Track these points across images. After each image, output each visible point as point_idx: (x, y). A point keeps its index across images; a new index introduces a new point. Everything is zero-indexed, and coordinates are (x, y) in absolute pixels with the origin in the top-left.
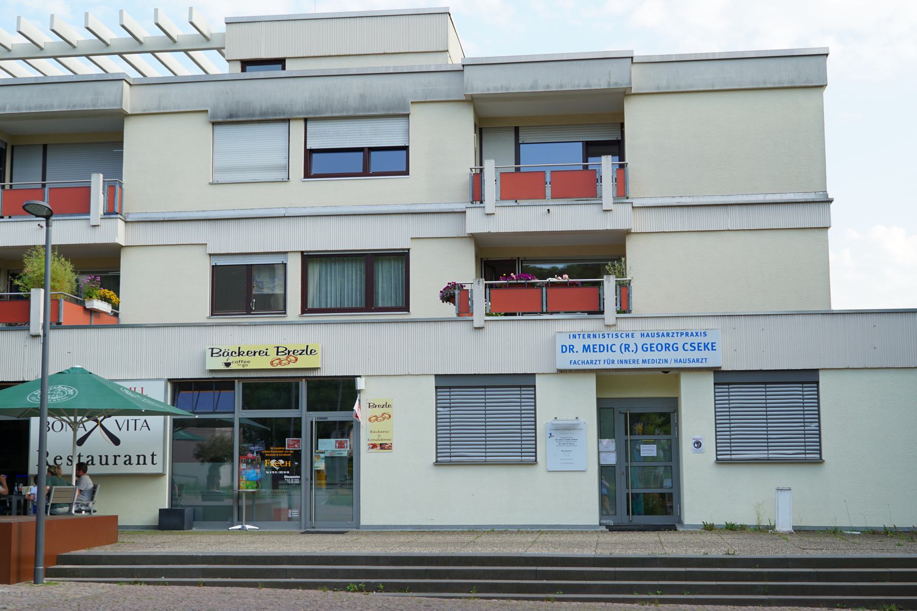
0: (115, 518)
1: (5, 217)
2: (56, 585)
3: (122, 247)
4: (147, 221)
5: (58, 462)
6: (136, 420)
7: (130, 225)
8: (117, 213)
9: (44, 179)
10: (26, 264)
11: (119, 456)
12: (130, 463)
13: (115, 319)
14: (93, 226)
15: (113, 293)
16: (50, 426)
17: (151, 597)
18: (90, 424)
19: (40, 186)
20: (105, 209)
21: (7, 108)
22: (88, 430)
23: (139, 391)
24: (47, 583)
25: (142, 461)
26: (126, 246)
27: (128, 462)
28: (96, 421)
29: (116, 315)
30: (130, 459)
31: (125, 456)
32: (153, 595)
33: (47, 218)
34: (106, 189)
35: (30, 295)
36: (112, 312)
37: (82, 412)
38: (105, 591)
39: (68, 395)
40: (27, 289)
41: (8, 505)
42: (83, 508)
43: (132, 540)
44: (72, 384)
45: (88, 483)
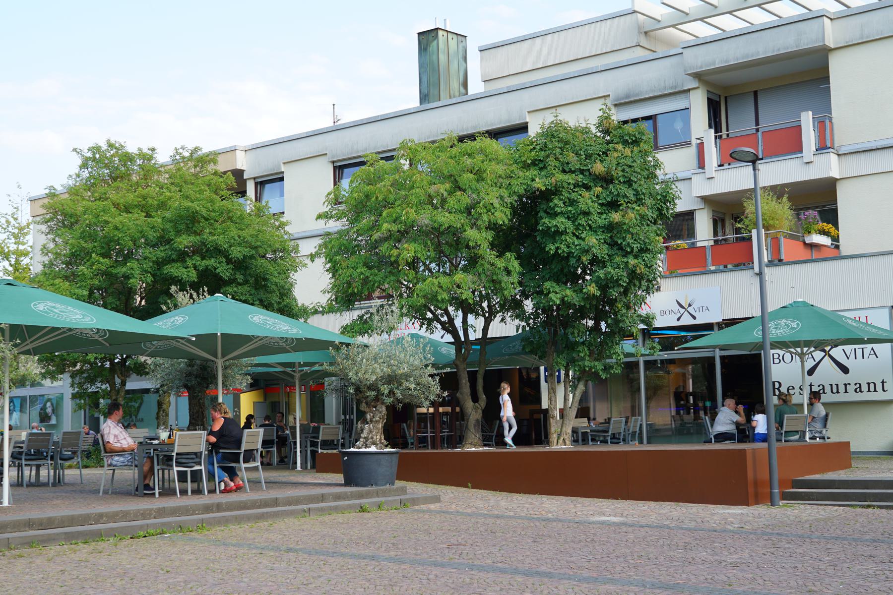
0: (847, 444)
1: (725, 165)
2: (792, 508)
3: (837, 180)
4: (859, 152)
5: (791, 392)
6: (863, 349)
7: (843, 157)
8: (830, 148)
9: (757, 124)
10: (745, 207)
11: (849, 384)
12: (861, 391)
13: (836, 250)
14: (806, 163)
15: (831, 226)
16: (781, 358)
17: (882, 520)
18: (818, 355)
19: (754, 131)
20: (817, 145)
21: (717, 63)
22: (817, 361)
23: (863, 320)
24: (783, 506)
25: (872, 389)
26: (840, 179)
27: (859, 389)
28: (824, 351)
29: (837, 247)
30: (860, 387)
31: (855, 384)
32: (885, 518)
33: (754, 162)
34: (816, 125)
35: (751, 236)
36: (832, 244)
37: (808, 344)
38: (837, 513)
39: (792, 328)
40: (748, 231)
41: (748, 433)
42: (817, 435)
43: (866, 466)
44: (795, 317)
45: (820, 410)
